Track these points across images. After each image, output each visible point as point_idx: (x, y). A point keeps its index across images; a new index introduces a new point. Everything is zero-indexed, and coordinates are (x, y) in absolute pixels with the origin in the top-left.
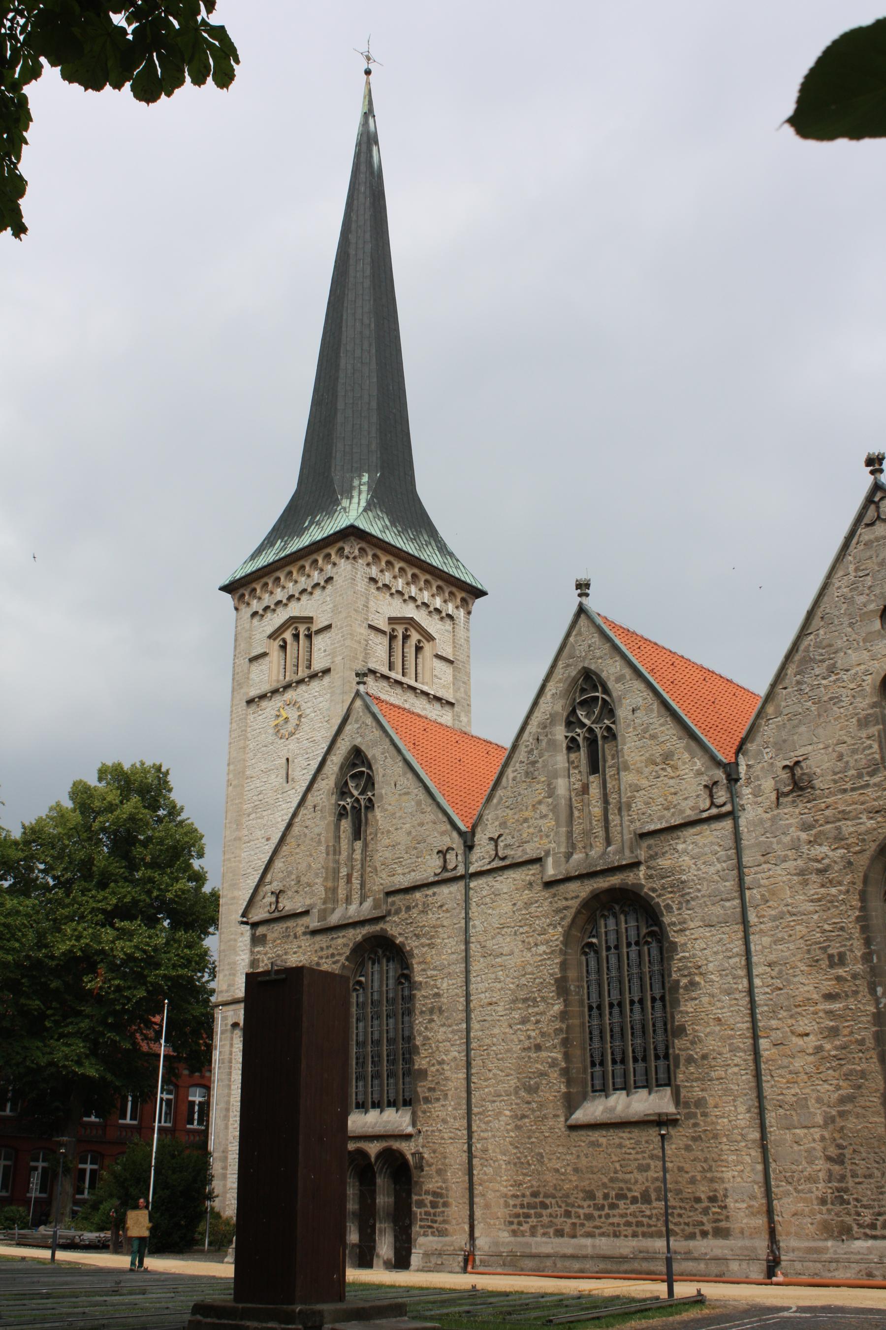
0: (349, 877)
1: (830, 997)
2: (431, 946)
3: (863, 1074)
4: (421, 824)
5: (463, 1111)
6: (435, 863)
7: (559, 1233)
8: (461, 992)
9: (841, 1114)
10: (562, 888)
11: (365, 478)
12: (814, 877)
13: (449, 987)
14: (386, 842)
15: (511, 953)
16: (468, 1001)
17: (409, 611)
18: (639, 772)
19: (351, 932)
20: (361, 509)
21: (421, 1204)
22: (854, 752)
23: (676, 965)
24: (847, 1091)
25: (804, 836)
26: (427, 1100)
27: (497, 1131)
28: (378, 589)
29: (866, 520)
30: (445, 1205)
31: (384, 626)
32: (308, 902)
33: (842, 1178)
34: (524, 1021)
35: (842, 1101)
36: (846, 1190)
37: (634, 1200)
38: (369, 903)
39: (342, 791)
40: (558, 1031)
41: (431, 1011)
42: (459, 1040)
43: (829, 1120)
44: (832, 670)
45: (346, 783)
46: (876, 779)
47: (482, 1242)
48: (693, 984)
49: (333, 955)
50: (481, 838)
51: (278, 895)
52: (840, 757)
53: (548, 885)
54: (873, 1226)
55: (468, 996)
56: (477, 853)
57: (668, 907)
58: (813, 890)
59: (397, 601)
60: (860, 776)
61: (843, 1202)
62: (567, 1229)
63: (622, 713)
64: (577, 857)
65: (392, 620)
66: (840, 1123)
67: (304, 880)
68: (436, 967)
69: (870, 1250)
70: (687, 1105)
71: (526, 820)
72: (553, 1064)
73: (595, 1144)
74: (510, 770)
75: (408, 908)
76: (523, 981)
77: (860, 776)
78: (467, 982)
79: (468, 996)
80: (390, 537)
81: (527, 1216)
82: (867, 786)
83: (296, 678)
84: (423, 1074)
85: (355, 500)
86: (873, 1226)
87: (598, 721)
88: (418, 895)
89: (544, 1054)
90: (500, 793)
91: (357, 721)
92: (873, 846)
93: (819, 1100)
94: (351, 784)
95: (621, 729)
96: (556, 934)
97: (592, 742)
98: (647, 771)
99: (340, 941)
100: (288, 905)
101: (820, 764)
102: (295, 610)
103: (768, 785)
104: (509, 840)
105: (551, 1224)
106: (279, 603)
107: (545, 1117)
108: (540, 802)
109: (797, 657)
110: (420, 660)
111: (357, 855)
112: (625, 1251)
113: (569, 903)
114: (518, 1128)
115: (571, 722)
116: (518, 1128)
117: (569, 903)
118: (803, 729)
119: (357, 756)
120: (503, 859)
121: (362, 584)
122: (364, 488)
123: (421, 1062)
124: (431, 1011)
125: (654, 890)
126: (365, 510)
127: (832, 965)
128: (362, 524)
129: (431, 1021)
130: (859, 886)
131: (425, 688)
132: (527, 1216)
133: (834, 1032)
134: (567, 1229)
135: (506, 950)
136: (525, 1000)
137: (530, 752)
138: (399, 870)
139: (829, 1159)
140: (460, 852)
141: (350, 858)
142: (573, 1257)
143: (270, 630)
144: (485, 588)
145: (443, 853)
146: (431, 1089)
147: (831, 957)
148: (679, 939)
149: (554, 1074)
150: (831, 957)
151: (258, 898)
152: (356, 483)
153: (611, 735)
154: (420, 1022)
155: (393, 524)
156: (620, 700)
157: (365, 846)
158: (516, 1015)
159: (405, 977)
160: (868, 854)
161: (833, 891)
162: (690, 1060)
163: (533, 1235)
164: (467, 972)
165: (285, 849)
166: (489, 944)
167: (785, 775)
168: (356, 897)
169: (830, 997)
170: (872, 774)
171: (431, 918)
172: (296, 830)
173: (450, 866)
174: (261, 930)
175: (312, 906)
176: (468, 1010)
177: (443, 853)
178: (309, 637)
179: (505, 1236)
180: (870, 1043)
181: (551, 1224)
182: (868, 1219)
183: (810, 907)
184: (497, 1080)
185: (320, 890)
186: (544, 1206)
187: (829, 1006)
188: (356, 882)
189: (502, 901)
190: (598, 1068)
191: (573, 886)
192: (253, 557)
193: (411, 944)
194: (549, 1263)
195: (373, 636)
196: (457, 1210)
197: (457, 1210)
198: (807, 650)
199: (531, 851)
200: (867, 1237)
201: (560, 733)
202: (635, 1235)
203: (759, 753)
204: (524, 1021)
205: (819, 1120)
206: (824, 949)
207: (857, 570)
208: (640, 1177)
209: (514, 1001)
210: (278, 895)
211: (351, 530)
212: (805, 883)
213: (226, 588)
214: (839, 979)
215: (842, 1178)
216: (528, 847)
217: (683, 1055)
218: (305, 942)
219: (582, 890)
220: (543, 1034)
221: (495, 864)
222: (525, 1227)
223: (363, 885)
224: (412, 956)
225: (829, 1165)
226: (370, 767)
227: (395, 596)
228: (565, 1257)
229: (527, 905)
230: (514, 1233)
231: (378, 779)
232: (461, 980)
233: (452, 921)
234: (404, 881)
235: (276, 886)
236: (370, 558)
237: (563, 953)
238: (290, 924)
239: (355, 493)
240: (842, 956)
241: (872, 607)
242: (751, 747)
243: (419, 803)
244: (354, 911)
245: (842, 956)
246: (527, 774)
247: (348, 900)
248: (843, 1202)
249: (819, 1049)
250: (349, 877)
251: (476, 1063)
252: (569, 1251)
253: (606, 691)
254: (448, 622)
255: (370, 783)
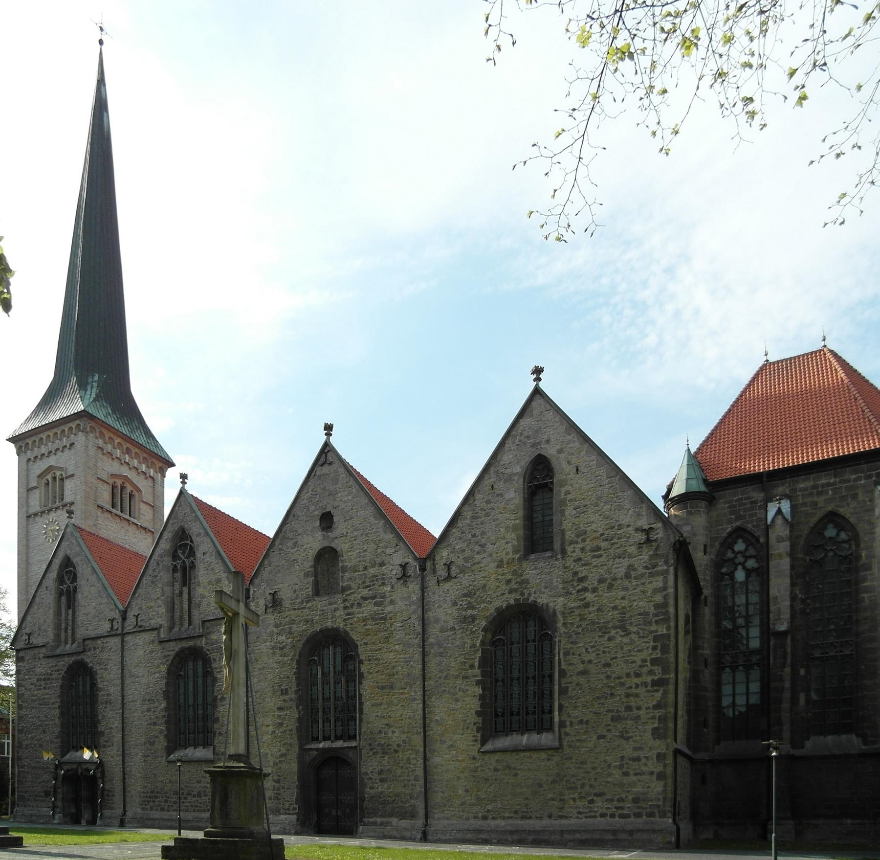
0: (66, 628)
1: (280, 709)
2: (106, 669)
3: (291, 745)
4: (101, 604)
5: (120, 752)
6: (107, 626)
7: (163, 810)
8: (120, 694)
9: (280, 761)
10: (167, 644)
11: (96, 378)
12: (278, 651)
13: (114, 691)
14: (83, 611)
15: (143, 676)
16: (123, 699)
17: (125, 471)
18: (205, 587)
19: (66, 659)
20: (92, 399)
21: (294, 809)
22: (301, 590)
23: (216, 688)
24: (283, 750)
25: (275, 630)
26: (104, 746)
27: (137, 762)
28: (104, 454)
29: (320, 463)
30: (113, 796)
31: (105, 477)
32: (45, 640)
33: (278, 789)
34: (149, 710)
35: (282, 755)
36: (279, 794)
37: (194, 796)
38: (74, 645)
39: (60, 580)
40: (163, 716)
41: (106, 703)
42: (118, 718)
43: (276, 764)
44: (295, 544)
45: (63, 576)
46: (309, 605)
47: (129, 813)
48: (223, 699)
49: (58, 670)
50: (131, 614)
51: (29, 635)
52: (295, 591)
53: (161, 642)
54: (289, 809)
55: (123, 696)
56: (128, 623)
57: (215, 660)
58: (278, 658)
59: (116, 464)
60: (302, 602)
61: (278, 799)
62: (166, 808)
63: (199, 555)
64: (176, 629)
65: (113, 476)
66: (280, 765)
67: (43, 628)
68: (108, 679)
69: (286, 819)
70: (218, 754)
71: (151, 607)
72: (161, 732)
73: (416, 779)
74: (144, 579)
75: (95, 649)
76: (148, 691)
77: (302, 602)
78: (123, 690)
79: (123, 696)
80: (110, 421)
81: (149, 801)
82: (304, 608)
83: (54, 506)
84: (102, 733)
85: (89, 392)
86: (289, 809)
87: (188, 557)
88: (99, 642)
89: (157, 727)
90: (139, 591)
91: (68, 540)
92: (305, 638)
93: (272, 755)
94: (66, 578)
95: (197, 563)
96: (164, 668)
97: (184, 569)
98: (208, 588)
99: (62, 663)
100: (35, 641)
101: (286, 594)
102: (52, 461)
103: (262, 602)
104: (144, 618)
105: (159, 806)
106: (43, 455)
107: (157, 757)
108: (158, 598)
109: (281, 536)
110: (132, 503)
111: (70, 617)
112: (190, 818)
113: (170, 653)
114: (145, 761)
115: (175, 557)
116: (145, 761)
117: (170, 653)
118: (279, 575)
119: (67, 562)
120: (141, 627)
121: (92, 451)
122: (95, 384)
123: (101, 728)
124: (106, 703)
125: (208, 650)
126: (94, 400)
127: (282, 694)
128: (91, 410)
129: (106, 707)
130: (297, 657)
131: (135, 521)
132: (149, 801)
133: (281, 724)
134: (166, 808)
135: (140, 675)
136: (149, 700)
137: (154, 570)
138: (90, 628)
139: (274, 781)
140: (120, 621)
141: (66, 619)
142: (168, 820)
143: (38, 472)
144: (175, 461)
145: (112, 621)
146: (106, 741)
147: (282, 690)
148: (219, 676)
149: (162, 737)
150: (282, 690)
151: (19, 636)
152: (90, 380)
153: (193, 566)
154: (101, 707)
155: (114, 412)
156: (198, 546)
157: (74, 613)
158: (145, 707)
159: (93, 685)
160: (302, 642)
161: (286, 659)
162: (220, 734)
163: (151, 810)
164: (123, 684)
165: (32, 610)
166: (133, 670)
167: (269, 597)
168: (70, 640)
169: (280, 709)
170: (307, 602)
171: (105, 656)
172: (37, 599)
173: (115, 628)
174: (21, 654)
175: (48, 643)
176: (123, 704)
177: (112, 621)
178: (62, 479)
179: (139, 810)
180: (294, 731)
181: (159, 806)
182: (287, 806)
183: (275, 665)
184: (136, 737)
185: (51, 634)
186: (156, 797)
187: (279, 713)
188: (70, 632)
189: (141, 648)
190: (182, 736)
191: (172, 644)
192: (29, 419)
193: (96, 667)
194: (157, 822)
195: (100, 485)
196: (118, 798)
197: (118, 798)
198: (285, 532)
199: (154, 623)
200: (286, 814)
201: (168, 561)
202: (194, 811)
203: (259, 585)
204: (149, 710)
205: (271, 764)
206: (280, 686)
207: (312, 490)
208: (198, 785)
209: (145, 700)
210: (29, 635)
211: (83, 413)
212: (274, 654)
213: (12, 440)
214: (284, 700)
215: (278, 789)
216: (153, 622)
217: (218, 731)
218: (44, 662)
219: (175, 647)
220: (157, 718)
221: (135, 630)
222: (148, 806)
223: (73, 634)
224: (97, 674)
225: (274, 783)
226: (75, 568)
227: (116, 460)
228: (164, 820)
229: (151, 652)
230: (143, 809)
231: (79, 575)
232: (119, 688)
233: (116, 658)
234: (93, 634)
235: (27, 630)
236: (98, 434)
237: (167, 678)
238: (36, 651)
239: (89, 388)
240: (287, 690)
241: (316, 513)
242: (256, 581)
243: (99, 591)
244: (69, 648)
245: (287, 690)
246: (152, 582)
247: (66, 642)
248: (278, 799)
249: (273, 732)
250: (66, 628)
251: (127, 729)
252: (166, 817)
253: (192, 541)
254: (150, 480)
255: (74, 578)
